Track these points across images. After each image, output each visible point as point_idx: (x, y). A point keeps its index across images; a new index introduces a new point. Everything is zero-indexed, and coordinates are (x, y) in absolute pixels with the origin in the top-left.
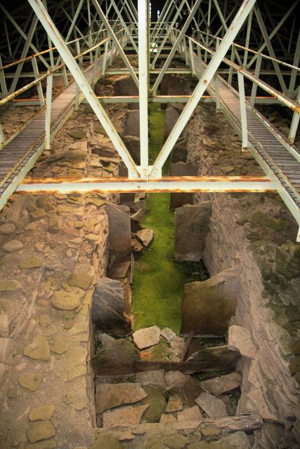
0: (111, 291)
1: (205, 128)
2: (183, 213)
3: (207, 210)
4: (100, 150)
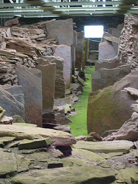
0: (11, 98)
2: (100, 78)
4: (16, 45)
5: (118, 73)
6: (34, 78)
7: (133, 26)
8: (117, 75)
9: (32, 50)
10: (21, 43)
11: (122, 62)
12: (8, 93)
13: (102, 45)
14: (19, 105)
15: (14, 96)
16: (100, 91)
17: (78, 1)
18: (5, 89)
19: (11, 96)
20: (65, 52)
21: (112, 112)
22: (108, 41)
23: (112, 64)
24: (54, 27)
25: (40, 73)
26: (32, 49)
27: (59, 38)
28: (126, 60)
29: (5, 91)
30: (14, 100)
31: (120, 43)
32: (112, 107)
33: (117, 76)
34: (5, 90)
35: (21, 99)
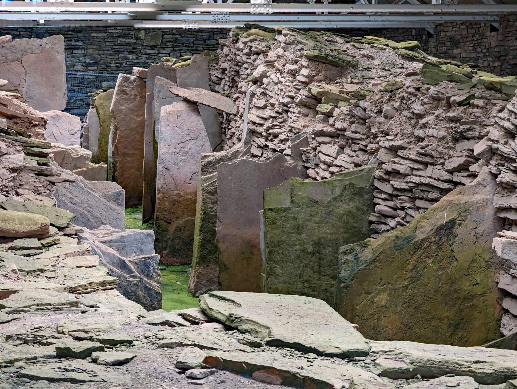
1: (311, 59)
3: (359, 192)
5: (338, 191)
6: (103, 207)
7: (311, 59)
8: (336, 196)
9: (35, 125)
10: (5, 105)
11: (293, 158)
12: (111, 251)
13: (169, 114)
14: (146, 287)
15: (131, 259)
16: (369, 241)
17: (249, 1)
18: (101, 239)
19: (124, 261)
20: (63, 132)
21: (406, 300)
22: (186, 100)
23: (267, 165)
24: (10, 58)
25: (119, 194)
26: (37, 123)
27: (24, 90)
28: (308, 155)
29: (104, 247)
30: (130, 271)
31: (250, 108)
32: (406, 287)
33: (335, 198)
34: (102, 242)
35: (152, 268)
